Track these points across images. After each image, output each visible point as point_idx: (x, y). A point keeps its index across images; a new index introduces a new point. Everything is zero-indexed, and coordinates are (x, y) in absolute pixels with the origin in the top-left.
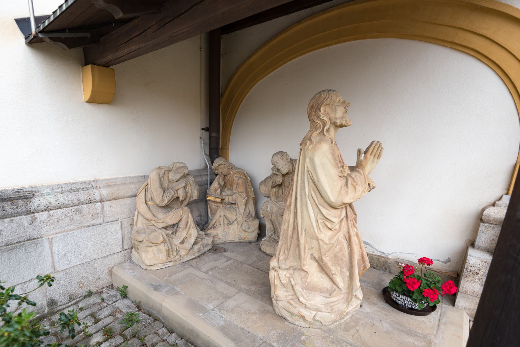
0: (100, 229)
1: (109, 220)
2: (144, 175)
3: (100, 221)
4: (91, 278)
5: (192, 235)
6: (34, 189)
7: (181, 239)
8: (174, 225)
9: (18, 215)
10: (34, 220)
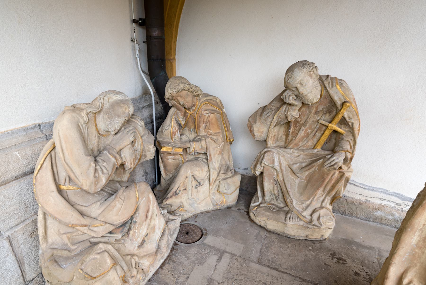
2: (40, 122)
5: (157, 227)
7: (140, 240)
8: (124, 224)
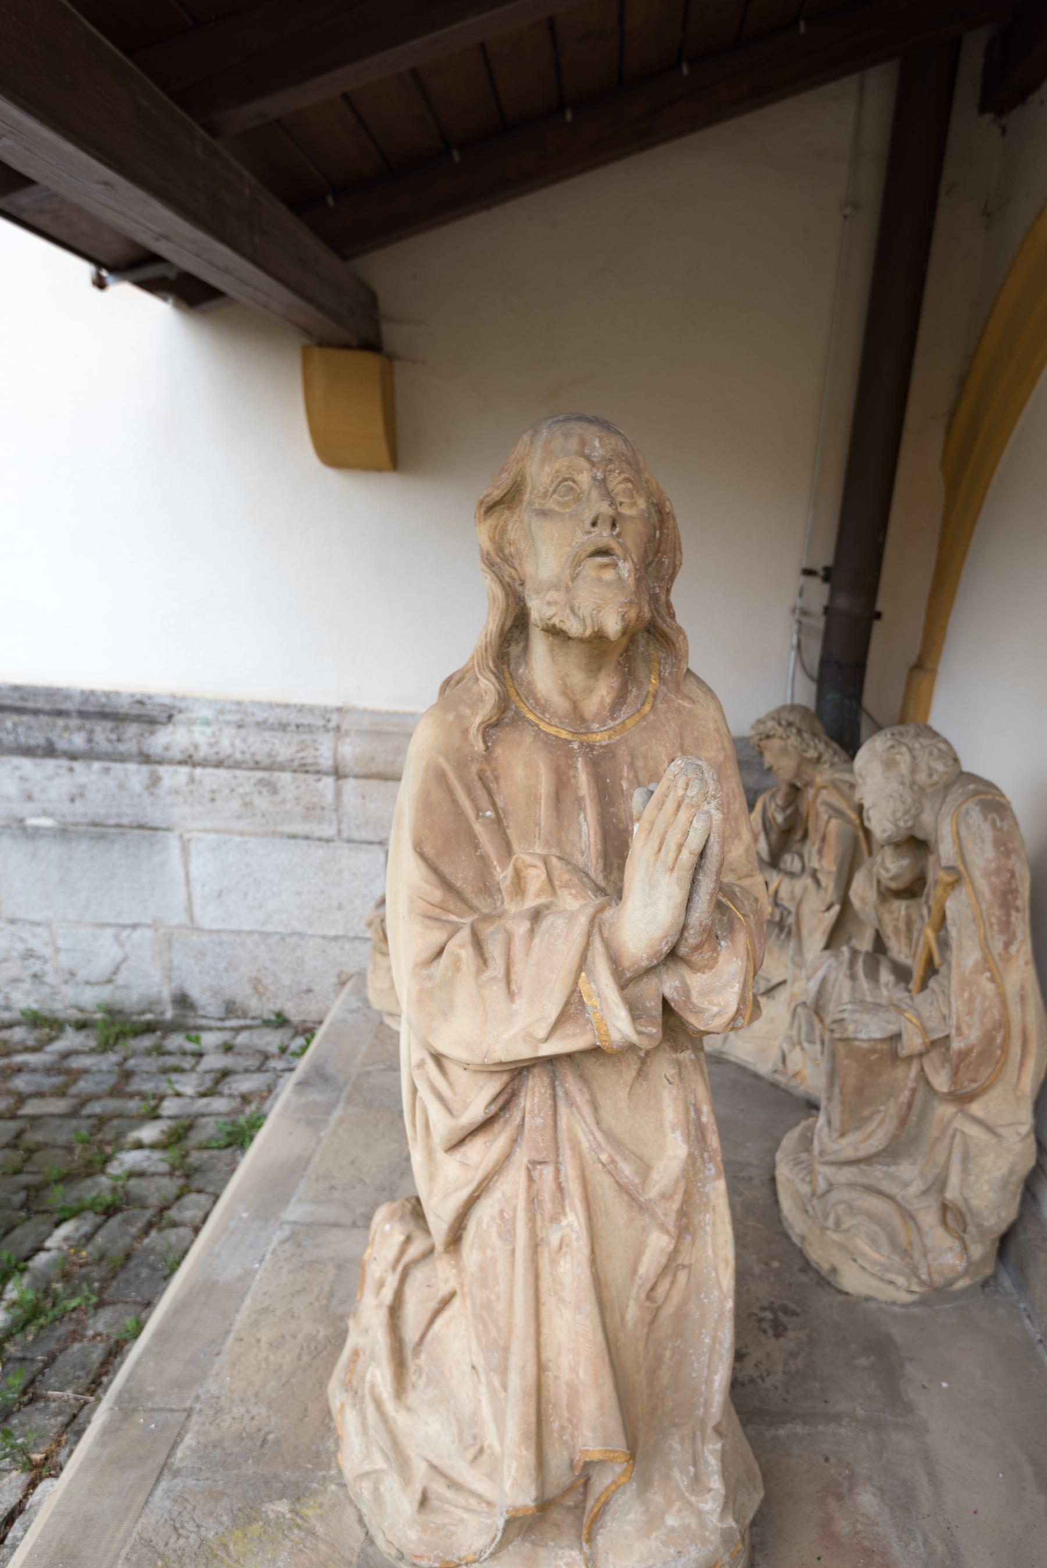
0: (319, 852)
1: (355, 835)
3: (329, 831)
4: (286, 980)
6: (178, 704)
9: (122, 758)
10: (155, 781)
